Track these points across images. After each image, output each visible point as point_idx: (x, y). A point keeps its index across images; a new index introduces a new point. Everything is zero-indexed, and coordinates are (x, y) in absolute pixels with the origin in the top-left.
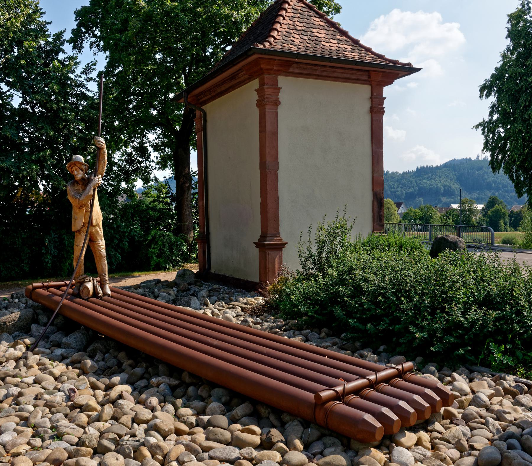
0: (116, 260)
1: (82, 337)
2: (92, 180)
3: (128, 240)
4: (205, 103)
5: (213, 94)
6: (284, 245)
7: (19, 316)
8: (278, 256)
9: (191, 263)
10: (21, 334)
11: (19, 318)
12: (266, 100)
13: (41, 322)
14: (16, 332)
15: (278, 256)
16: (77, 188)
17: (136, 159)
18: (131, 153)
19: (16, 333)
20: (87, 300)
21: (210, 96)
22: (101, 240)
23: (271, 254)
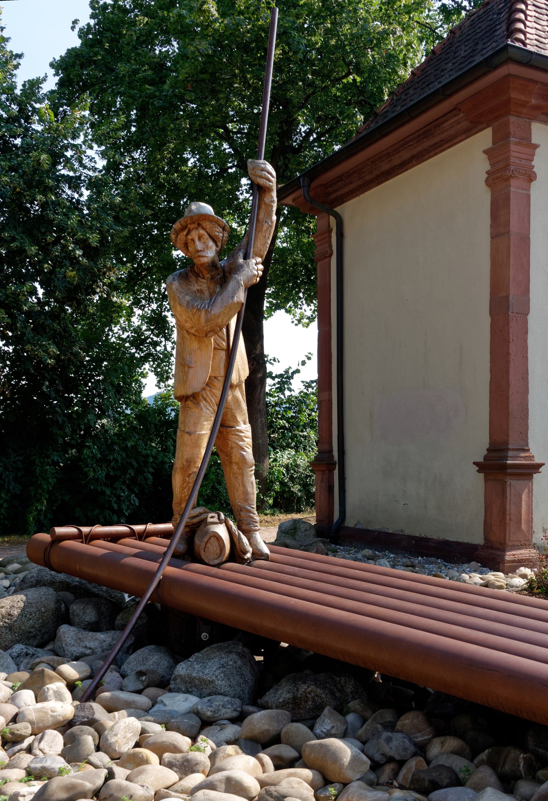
0: (128, 507)
1: (239, 663)
2: (241, 266)
3: (152, 470)
4: (342, 200)
5: (369, 177)
6: (537, 467)
7: (22, 604)
8: (526, 491)
9: (266, 515)
10: (31, 650)
11: (23, 610)
12: (512, 168)
13: (77, 620)
14: (32, 644)
15: (526, 491)
16: (196, 287)
17: (148, 337)
18: (139, 327)
19: (18, 648)
20: (218, 566)
21: (360, 182)
22: (245, 424)
23: (514, 484)
